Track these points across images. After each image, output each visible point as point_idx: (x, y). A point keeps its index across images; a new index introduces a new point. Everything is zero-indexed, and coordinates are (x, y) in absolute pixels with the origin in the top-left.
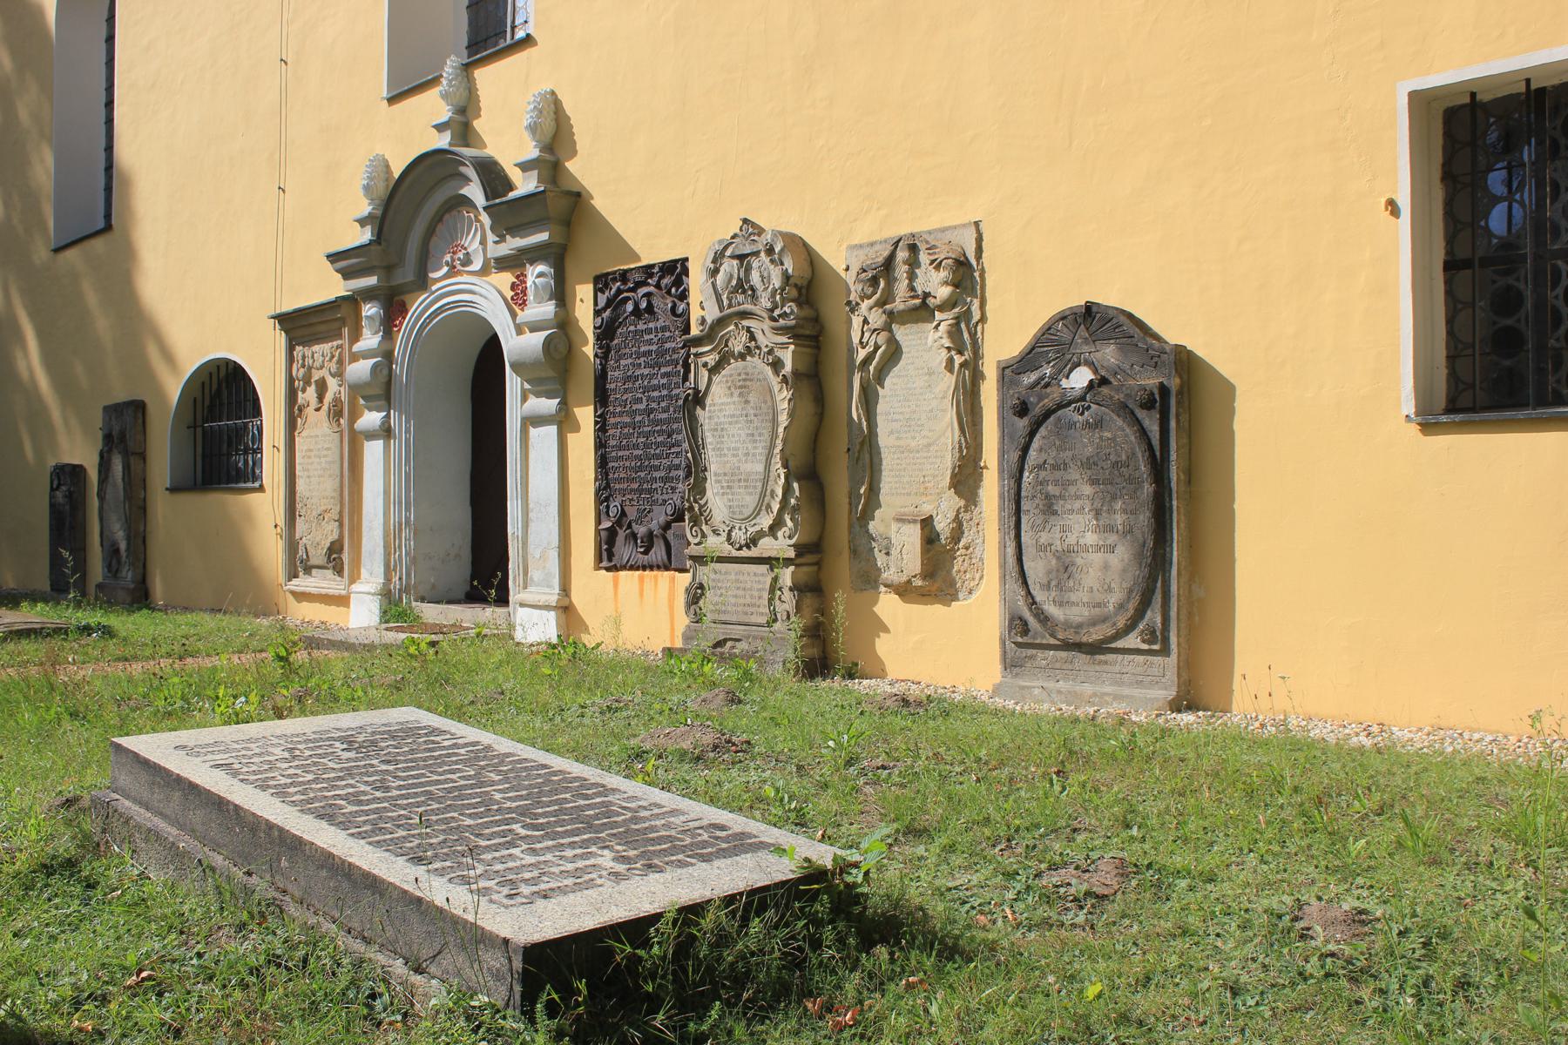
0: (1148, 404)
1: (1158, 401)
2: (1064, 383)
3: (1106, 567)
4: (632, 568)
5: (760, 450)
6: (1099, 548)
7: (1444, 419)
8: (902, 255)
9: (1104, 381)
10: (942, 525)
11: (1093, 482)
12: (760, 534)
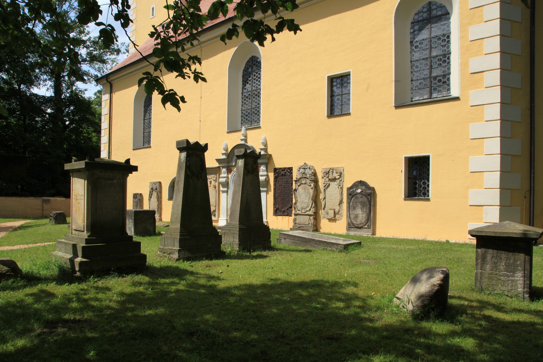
0: (369, 195)
1: (370, 195)
2: (357, 191)
3: (362, 216)
4: (280, 216)
5: (308, 198)
6: (361, 214)
7: (408, 198)
8: (331, 171)
9: (362, 191)
10: (337, 210)
11: (361, 205)
12: (307, 211)
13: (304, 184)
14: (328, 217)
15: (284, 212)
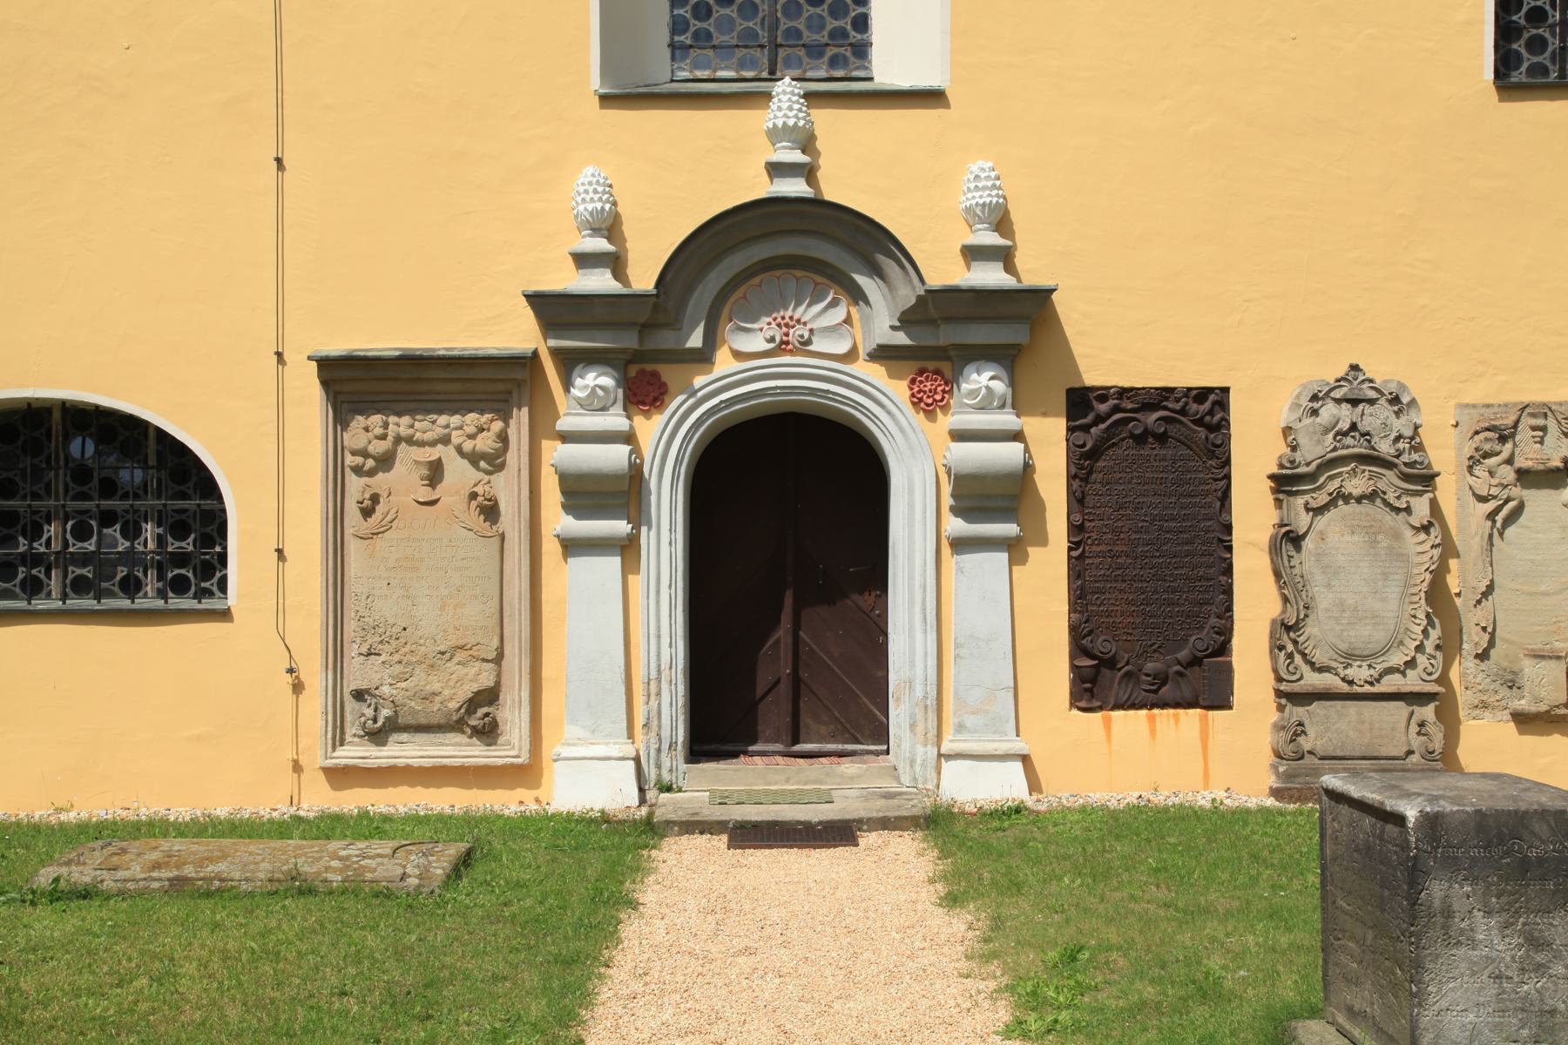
12: (1390, 671)
13: (1359, 500)
14: (1523, 704)
15: (1161, 679)
